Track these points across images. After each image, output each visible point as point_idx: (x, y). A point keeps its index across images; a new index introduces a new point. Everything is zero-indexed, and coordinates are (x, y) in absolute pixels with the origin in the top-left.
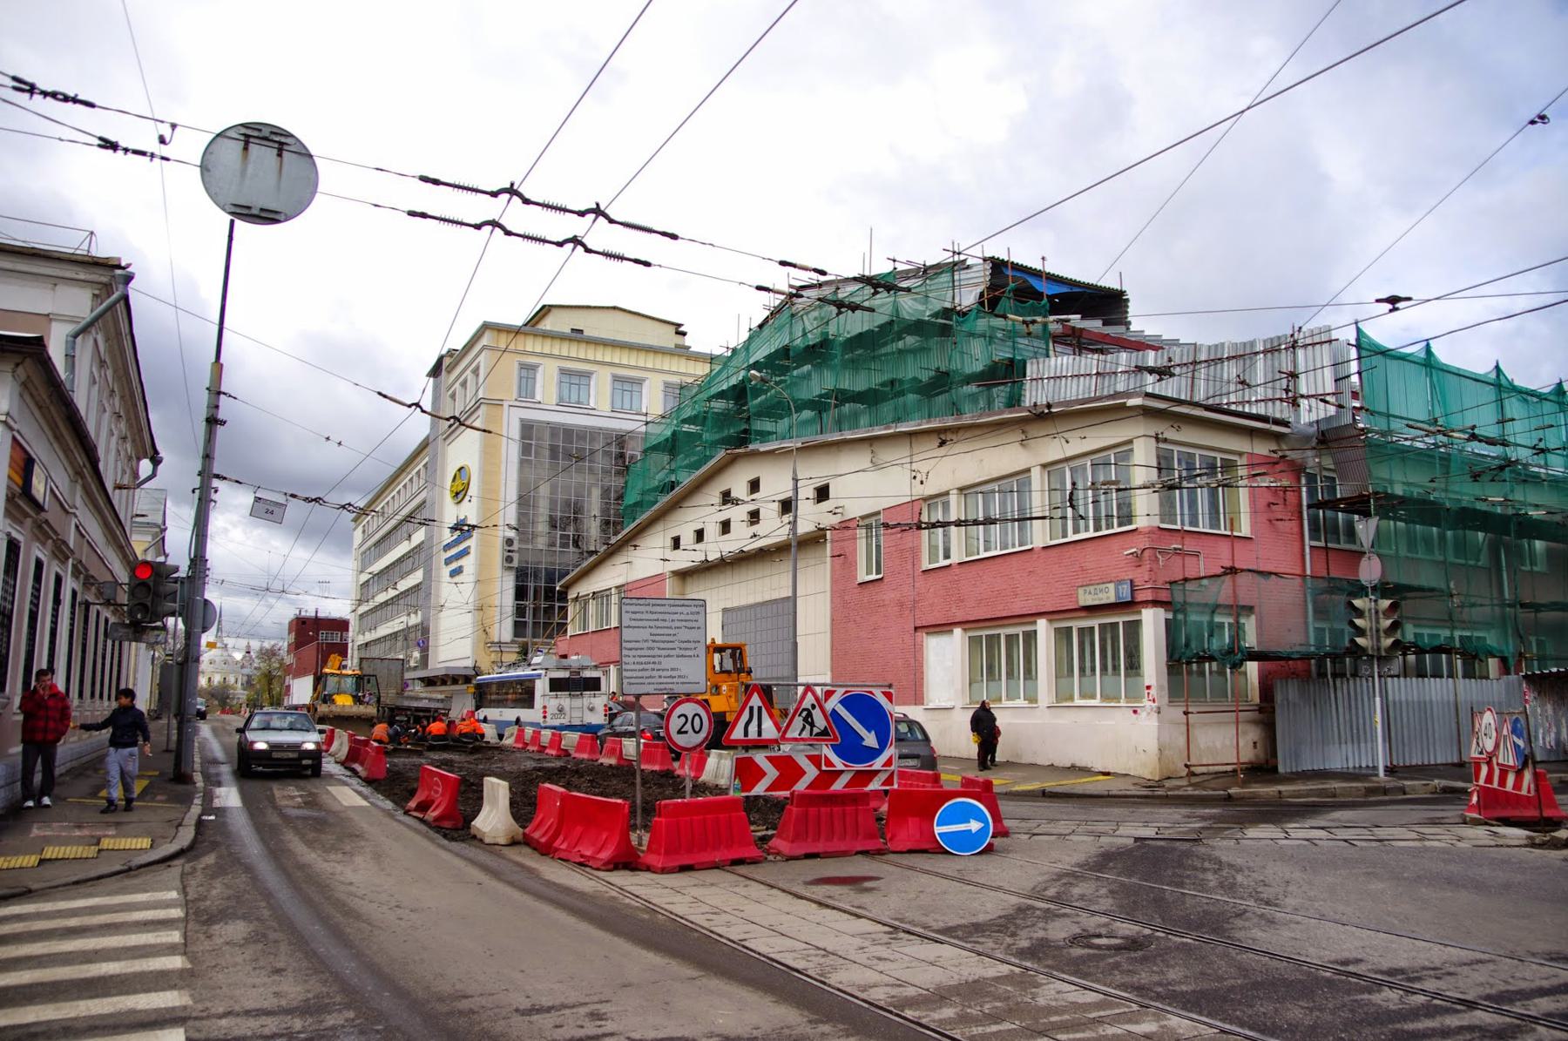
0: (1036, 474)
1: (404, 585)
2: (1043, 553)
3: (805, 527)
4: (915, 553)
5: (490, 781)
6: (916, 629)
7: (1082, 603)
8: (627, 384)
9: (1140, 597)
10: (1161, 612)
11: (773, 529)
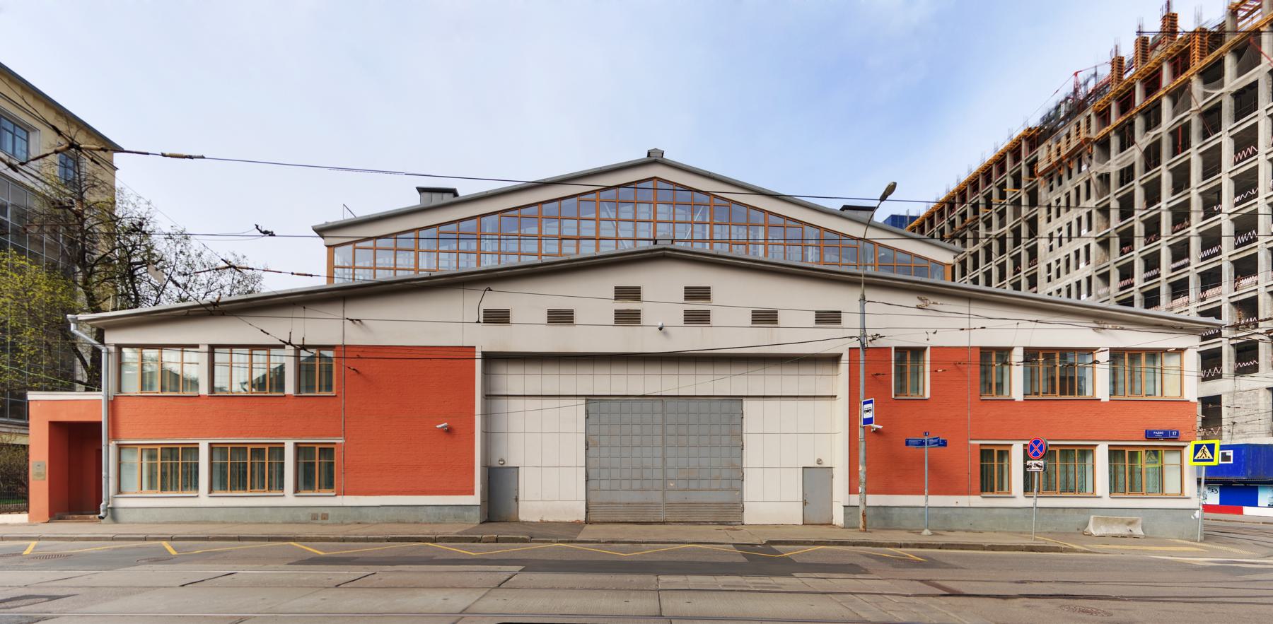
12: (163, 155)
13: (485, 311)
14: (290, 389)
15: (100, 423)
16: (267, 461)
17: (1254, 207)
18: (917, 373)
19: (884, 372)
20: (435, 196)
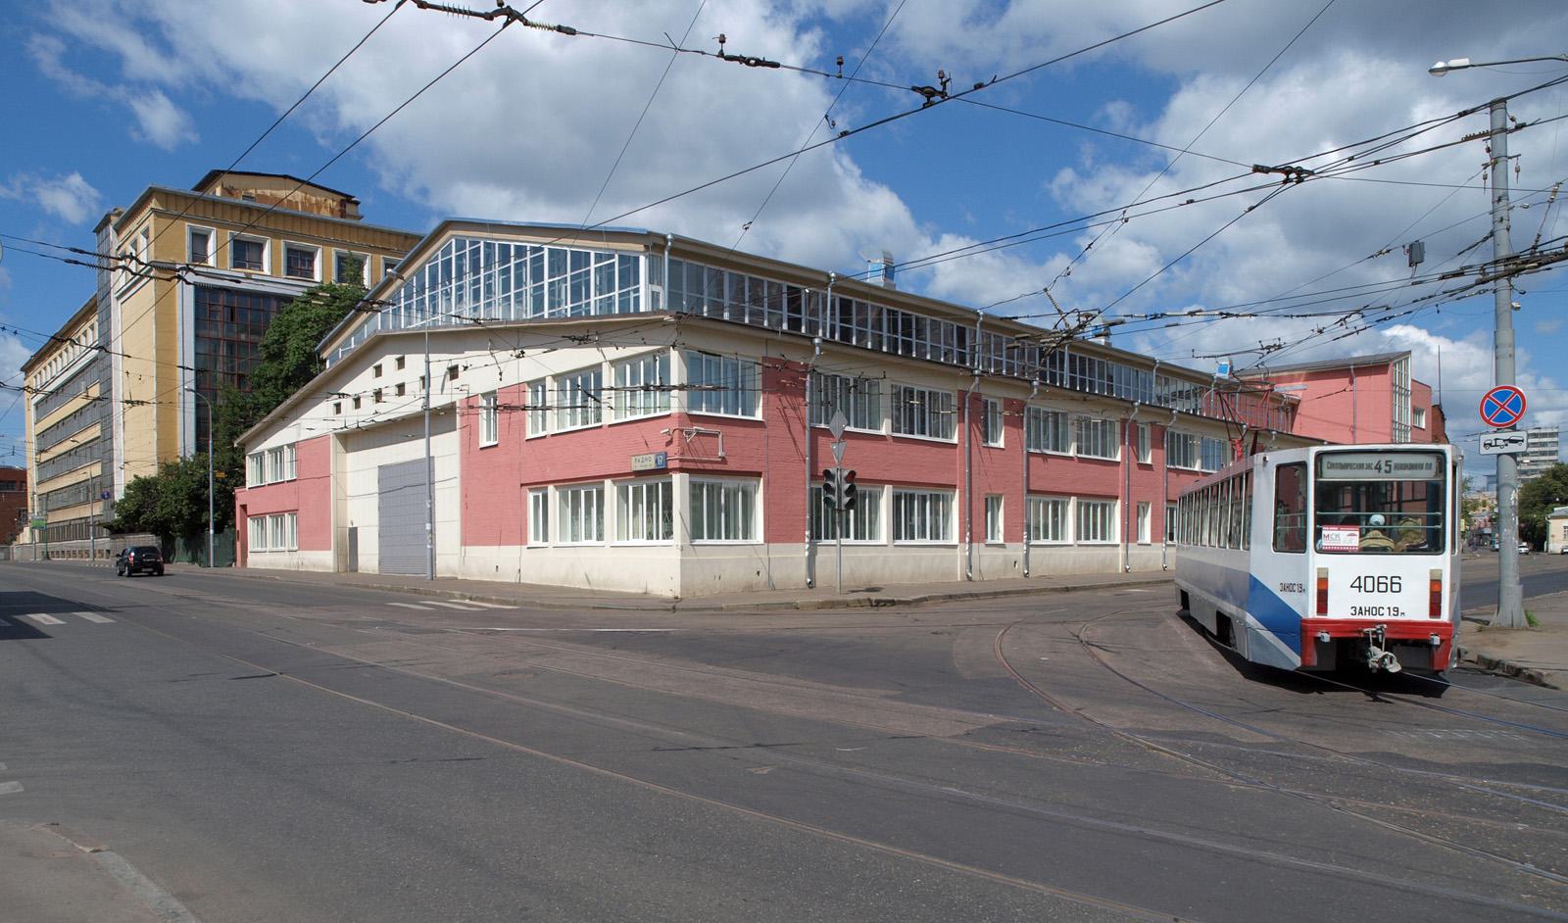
0: (606, 367)
1: (82, 438)
3: (436, 402)
6: (522, 485)
7: (634, 469)
8: (298, 262)
9: (671, 465)
11: (410, 405)
12: (703, 53)
13: (1319, 569)
14: (468, 242)
15: (23, 473)
16: (928, 343)
17: (641, 535)
18: (946, 516)
19: (1321, 521)
20: (973, 451)
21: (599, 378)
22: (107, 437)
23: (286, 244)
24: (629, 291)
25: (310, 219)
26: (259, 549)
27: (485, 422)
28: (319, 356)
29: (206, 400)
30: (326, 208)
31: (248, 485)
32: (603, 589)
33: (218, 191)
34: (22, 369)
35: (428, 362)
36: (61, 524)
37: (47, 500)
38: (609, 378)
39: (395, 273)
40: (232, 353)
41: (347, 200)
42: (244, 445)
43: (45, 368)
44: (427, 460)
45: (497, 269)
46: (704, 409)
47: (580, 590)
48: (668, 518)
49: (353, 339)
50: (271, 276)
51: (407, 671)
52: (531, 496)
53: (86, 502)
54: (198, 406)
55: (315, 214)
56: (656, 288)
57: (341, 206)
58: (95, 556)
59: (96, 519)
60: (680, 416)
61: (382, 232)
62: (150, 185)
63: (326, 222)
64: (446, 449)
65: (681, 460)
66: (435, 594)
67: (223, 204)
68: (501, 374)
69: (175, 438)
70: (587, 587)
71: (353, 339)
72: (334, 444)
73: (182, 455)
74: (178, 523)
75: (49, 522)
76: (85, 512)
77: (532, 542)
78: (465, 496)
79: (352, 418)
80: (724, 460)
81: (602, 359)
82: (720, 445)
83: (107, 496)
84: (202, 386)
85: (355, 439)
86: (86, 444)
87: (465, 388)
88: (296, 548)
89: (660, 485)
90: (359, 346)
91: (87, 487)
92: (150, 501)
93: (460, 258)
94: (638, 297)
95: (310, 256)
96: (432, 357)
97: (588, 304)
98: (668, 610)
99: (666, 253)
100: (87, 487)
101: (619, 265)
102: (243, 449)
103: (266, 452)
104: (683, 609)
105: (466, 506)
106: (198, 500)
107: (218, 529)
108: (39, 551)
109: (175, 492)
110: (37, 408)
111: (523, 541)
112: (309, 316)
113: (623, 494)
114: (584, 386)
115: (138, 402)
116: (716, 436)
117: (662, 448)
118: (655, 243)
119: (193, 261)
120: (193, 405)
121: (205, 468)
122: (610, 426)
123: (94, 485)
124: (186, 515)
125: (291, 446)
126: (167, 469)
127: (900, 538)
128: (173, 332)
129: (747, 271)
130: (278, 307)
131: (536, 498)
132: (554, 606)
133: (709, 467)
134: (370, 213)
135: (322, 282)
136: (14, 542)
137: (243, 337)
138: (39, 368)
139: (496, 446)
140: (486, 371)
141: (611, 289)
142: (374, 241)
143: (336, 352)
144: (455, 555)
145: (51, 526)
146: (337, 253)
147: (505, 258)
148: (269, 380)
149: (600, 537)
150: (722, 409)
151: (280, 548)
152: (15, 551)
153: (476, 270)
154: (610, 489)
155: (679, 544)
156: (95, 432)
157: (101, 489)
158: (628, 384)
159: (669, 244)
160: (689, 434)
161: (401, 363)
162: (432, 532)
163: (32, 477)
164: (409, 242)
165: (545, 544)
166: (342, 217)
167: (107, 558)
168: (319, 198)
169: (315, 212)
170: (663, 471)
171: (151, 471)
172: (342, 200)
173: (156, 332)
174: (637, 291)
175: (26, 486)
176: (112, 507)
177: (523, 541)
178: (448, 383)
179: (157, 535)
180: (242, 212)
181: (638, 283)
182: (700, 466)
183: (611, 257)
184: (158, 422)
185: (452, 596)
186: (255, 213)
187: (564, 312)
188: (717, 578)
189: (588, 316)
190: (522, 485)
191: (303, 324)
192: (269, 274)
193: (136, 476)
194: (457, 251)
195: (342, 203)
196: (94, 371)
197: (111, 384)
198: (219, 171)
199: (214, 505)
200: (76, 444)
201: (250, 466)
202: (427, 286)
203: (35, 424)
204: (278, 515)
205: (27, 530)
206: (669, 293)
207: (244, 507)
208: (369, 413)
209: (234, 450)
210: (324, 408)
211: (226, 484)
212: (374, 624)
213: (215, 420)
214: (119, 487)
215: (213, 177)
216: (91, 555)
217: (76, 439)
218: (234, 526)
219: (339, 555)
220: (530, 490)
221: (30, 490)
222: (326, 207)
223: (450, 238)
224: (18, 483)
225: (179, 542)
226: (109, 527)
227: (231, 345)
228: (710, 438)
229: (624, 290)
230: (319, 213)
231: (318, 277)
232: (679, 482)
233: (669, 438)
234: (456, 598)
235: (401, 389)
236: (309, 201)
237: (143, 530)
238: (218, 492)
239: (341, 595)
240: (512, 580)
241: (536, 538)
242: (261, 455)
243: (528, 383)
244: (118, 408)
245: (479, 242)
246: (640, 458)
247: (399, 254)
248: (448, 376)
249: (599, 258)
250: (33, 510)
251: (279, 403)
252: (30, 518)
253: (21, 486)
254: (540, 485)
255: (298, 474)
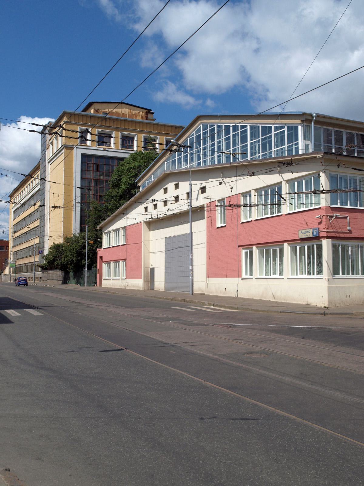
0: (284, 184)
1: (32, 226)
2: (286, 216)
3: (195, 204)
4: (239, 215)
5: (298, 246)
6: (239, 246)
8: (127, 142)
9: (321, 235)
10: (330, 240)
11: (182, 206)
14: (209, 125)
15: (7, 242)
21: (280, 189)
22: (42, 226)
23: (122, 134)
24: (292, 145)
25: (132, 122)
26: (107, 278)
27: (219, 214)
28: (137, 184)
29: (85, 207)
30: (140, 115)
31: (103, 247)
32: (283, 301)
33: (92, 111)
34: (9, 196)
35: (191, 185)
36: (22, 265)
37: (16, 254)
38: (285, 189)
39: (175, 141)
40: (97, 185)
41: (149, 112)
42: (102, 228)
43: (18, 195)
44: (190, 234)
45: (223, 138)
46: (339, 204)
47: (270, 302)
48: (320, 264)
49: (153, 176)
50: (115, 149)
51: (193, 349)
52: (243, 252)
53: (32, 255)
54: (82, 210)
55: (134, 119)
56: (308, 142)
57: (146, 114)
58: (35, 280)
59: (36, 263)
60: (326, 208)
61: (165, 126)
62: (64, 111)
63: (139, 122)
64: (199, 229)
65: (327, 232)
66: (195, 302)
67: (94, 117)
68: (231, 188)
69: (71, 226)
70: (273, 300)
71: (153, 176)
72: (144, 227)
73: (74, 233)
74: (71, 265)
75: (16, 264)
76: (32, 260)
77: (244, 276)
78: (209, 252)
79: (153, 214)
80: (350, 232)
81: (281, 180)
82: (348, 223)
83: (41, 252)
84: (83, 201)
85: (154, 224)
86: (33, 229)
87: (210, 197)
88: (125, 277)
89: (315, 245)
90: (156, 179)
91: (33, 248)
92: (59, 255)
93: (205, 134)
94: (298, 147)
95: (132, 139)
96: (193, 183)
97: (271, 153)
98: (321, 314)
99: (313, 123)
100: (33, 248)
101: (287, 131)
102: (102, 230)
103: (112, 231)
104: (331, 314)
105: (209, 258)
106: (80, 254)
107: (89, 269)
108: (12, 278)
109: (70, 251)
110: (14, 213)
111: (239, 275)
112: (131, 166)
113: (294, 250)
114: (273, 194)
115: (57, 207)
116: (346, 218)
117: (316, 226)
118: (306, 118)
119: (81, 144)
120: (79, 210)
121: (84, 239)
122: (287, 215)
123: (36, 248)
124: (77, 260)
125: (124, 228)
126: (67, 239)
127: (338, 274)
128: (72, 176)
129: (355, 130)
130: (118, 163)
131: (246, 253)
132: (259, 311)
133: (342, 235)
134: (159, 118)
135: (137, 151)
136: (2, 273)
137: (102, 178)
138: (16, 195)
139: (225, 226)
140: (217, 189)
141: (283, 144)
142: (161, 130)
143: (145, 182)
144: (203, 282)
145: (17, 266)
146: (144, 136)
147: (227, 132)
148: (112, 197)
149: (281, 273)
150: (349, 204)
151: (118, 278)
152: (2, 277)
153: (213, 139)
154: (287, 248)
155: (327, 277)
156: (37, 223)
157: (38, 249)
158: (296, 191)
159: (314, 118)
160: (331, 217)
161: (177, 186)
162: (192, 270)
163: (11, 244)
164: (177, 129)
165: (251, 277)
166: (146, 119)
167: (40, 281)
168: (136, 112)
169: (134, 118)
170: (317, 238)
171: (60, 241)
172: (147, 112)
173: (64, 176)
174: (297, 144)
175: (8, 248)
176: (43, 258)
177: (239, 275)
178: (200, 196)
179: (62, 271)
180: (102, 120)
181: (298, 140)
182: (337, 235)
183: (282, 127)
184: (64, 218)
185: (204, 304)
186: (108, 121)
187: (258, 157)
188: (348, 297)
189: (271, 157)
190: (239, 246)
191: (129, 170)
192: (114, 148)
193: (54, 243)
194: (203, 130)
195: (147, 113)
196: (37, 197)
197: (45, 202)
198: (93, 102)
199: (88, 257)
200: (29, 229)
201: (105, 238)
202: (195, 141)
203: (13, 220)
204: (117, 262)
205: (8, 268)
206: (315, 144)
207: (101, 258)
208: (162, 211)
209: (97, 230)
210: (140, 209)
211: (93, 247)
212: (168, 319)
213: (89, 217)
214: (47, 248)
215: (90, 105)
216: (33, 280)
217: (29, 226)
218: (96, 267)
219: (145, 281)
220: (243, 249)
221: (10, 250)
222: (139, 116)
223: (200, 124)
224: (5, 247)
225: (71, 274)
226: (41, 267)
227: (96, 181)
228: (343, 220)
229: (290, 144)
230: (136, 119)
231: (135, 148)
232: (326, 244)
233: (320, 220)
234: (206, 305)
235: (177, 198)
236: (132, 113)
237: (56, 269)
238: (89, 250)
239: (143, 302)
240: (234, 295)
241: (246, 274)
242: (109, 233)
243: (242, 194)
244: (47, 210)
245: (215, 125)
246: (304, 231)
247: (172, 135)
248: (200, 191)
249: (276, 129)
250: (11, 259)
251: (118, 208)
252: (9, 263)
253: (6, 248)
254: (248, 246)
255: (127, 242)
